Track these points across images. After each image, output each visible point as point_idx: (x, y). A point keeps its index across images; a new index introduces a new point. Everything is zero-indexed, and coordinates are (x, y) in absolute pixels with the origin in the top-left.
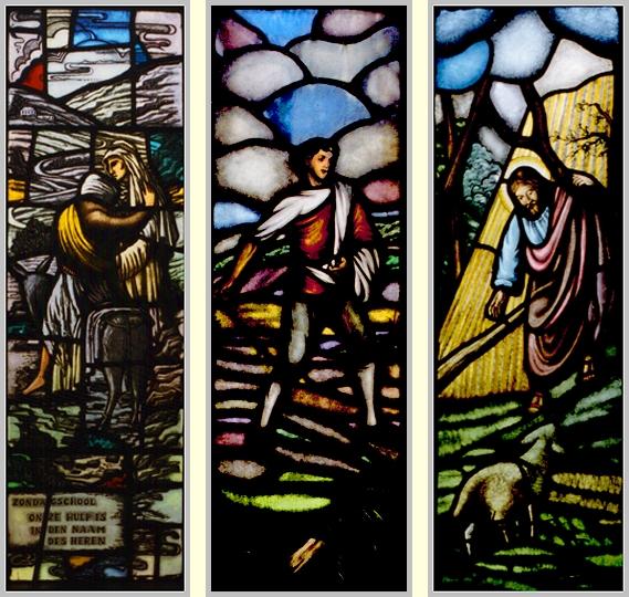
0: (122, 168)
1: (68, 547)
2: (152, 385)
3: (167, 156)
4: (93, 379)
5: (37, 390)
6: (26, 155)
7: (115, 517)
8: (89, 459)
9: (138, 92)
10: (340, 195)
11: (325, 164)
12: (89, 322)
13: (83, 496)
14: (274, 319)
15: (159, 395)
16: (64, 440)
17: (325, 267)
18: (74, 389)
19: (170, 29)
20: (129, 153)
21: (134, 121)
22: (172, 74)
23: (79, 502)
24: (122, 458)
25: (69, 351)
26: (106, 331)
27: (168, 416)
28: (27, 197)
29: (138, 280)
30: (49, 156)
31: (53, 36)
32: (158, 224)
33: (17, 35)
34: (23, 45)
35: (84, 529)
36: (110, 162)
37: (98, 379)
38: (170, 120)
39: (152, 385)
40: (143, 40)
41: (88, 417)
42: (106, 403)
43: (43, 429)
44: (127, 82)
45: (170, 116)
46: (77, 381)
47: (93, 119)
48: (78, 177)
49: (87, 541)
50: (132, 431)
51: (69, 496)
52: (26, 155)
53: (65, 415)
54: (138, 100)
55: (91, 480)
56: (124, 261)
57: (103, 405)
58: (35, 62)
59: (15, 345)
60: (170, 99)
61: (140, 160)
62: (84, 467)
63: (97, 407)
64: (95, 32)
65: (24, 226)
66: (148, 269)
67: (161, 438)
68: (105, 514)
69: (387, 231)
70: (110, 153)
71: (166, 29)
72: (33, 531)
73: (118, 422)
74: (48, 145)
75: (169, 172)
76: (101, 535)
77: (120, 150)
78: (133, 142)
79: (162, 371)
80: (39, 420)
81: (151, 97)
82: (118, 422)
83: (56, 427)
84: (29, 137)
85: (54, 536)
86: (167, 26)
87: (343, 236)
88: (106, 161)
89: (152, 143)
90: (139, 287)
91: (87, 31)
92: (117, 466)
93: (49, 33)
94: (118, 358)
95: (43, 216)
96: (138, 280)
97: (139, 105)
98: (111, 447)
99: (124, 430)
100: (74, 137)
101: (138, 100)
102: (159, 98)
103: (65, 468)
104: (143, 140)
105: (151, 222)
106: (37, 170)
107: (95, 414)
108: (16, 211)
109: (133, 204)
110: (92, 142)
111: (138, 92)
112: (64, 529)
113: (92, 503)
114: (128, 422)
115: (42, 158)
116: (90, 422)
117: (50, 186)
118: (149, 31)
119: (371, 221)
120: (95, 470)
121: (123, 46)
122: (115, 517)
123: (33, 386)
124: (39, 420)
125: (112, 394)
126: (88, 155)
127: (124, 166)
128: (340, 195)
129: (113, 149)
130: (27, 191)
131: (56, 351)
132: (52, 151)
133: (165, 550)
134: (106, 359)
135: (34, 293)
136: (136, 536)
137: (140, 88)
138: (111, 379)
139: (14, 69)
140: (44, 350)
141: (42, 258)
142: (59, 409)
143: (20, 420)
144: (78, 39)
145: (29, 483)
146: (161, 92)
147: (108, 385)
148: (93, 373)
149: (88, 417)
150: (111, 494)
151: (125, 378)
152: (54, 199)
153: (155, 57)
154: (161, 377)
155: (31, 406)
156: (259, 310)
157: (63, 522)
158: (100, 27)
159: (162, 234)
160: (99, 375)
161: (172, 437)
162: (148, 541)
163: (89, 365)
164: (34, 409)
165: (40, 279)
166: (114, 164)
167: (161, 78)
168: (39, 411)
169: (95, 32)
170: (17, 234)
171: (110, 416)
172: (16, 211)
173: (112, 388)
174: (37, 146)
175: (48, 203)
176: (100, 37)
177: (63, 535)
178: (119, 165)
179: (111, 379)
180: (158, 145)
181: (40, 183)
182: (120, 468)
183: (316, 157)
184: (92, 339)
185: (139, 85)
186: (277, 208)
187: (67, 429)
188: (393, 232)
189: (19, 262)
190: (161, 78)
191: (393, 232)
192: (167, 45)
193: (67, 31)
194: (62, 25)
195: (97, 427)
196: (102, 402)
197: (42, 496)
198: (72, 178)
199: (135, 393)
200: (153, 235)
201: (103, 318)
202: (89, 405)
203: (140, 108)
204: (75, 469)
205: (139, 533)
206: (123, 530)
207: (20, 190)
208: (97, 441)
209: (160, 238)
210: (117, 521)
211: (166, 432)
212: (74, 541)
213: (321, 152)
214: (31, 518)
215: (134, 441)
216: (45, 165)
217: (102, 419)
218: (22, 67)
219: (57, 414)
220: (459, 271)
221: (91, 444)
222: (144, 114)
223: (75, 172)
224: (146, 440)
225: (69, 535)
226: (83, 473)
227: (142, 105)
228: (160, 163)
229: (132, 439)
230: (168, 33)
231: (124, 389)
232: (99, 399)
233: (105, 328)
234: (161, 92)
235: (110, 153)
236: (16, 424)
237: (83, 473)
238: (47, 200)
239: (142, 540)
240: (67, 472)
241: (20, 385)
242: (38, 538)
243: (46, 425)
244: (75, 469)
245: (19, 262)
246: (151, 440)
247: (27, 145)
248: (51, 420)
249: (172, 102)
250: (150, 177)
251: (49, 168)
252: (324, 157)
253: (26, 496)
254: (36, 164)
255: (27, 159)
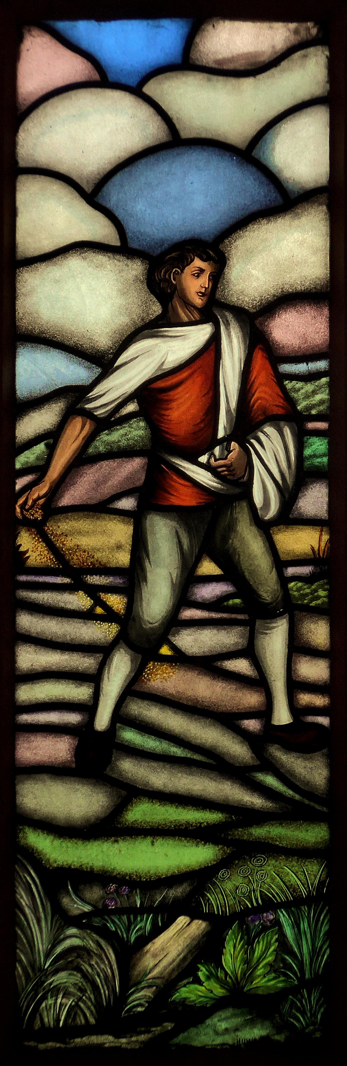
10: (229, 336)
11: (204, 281)
14: (119, 547)
17: (203, 459)
29: (220, 469)
69: (307, 396)
87: (233, 404)
96: (220, 469)
119: (284, 581)
128: (229, 336)
133: (319, 418)
156: (94, 533)
183: (188, 270)
186: (118, 363)
188: (318, 397)
191: (318, 397)
213: (198, 263)
252: (202, 271)
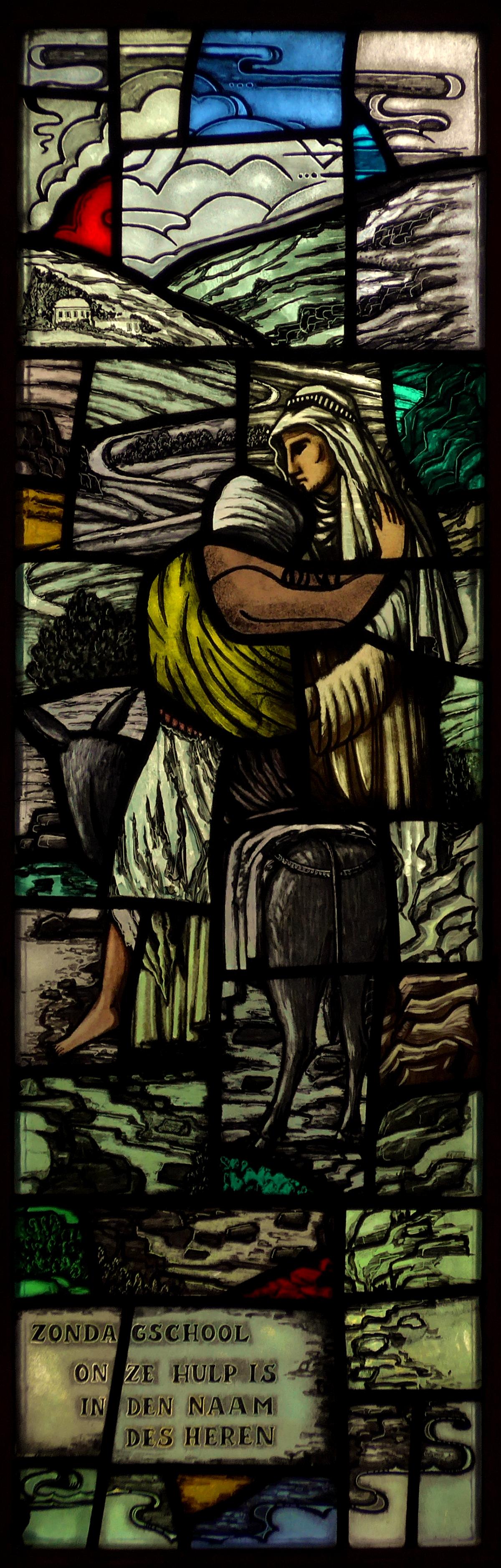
0: (320, 459)
1: (178, 1453)
2: (396, 1026)
3: (437, 426)
4: (240, 1012)
5: (97, 1041)
6: (66, 425)
7: (300, 1372)
8: (231, 1221)
9: (360, 255)
12: (232, 860)
13: (217, 1316)
15: (415, 1053)
16: (167, 1172)
18: (190, 1036)
19: (448, 86)
20: (337, 419)
21: (351, 332)
22: (453, 205)
23: (206, 1334)
24: (316, 1217)
25: (178, 936)
26: (278, 885)
27: (438, 1110)
28: (68, 533)
29: (362, 751)
30: (128, 426)
31: (138, 108)
32: (412, 603)
33: (42, 104)
34: (57, 131)
35: (219, 1406)
36: (288, 443)
37: (254, 1014)
38: (447, 330)
39: (396, 1026)
40: (376, 114)
41: (229, 1112)
42: (274, 1074)
43: (109, 1145)
44: (379, 379)
45: (447, 319)
46: (199, 1017)
47: (248, 329)
48: (203, 483)
49: (226, 1435)
50: (343, 1147)
51: (178, 1317)
52: (66, 425)
53: (168, 1107)
54: (362, 276)
55: (237, 1276)
56: (325, 701)
57: (268, 1081)
58: (91, 177)
59: (38, 923)
60: (446, 273)
61: (364, 436)
62: (217, 1240)
63: (254, 1085)
64: (250, 95)
65: (60, 611)
66: (387, 722)
67: (420, 1168)
68: (274, 1363)
70: (289, 420)
71: (439, 85)
72: (84, 1406)
73: (306, 1125)
74: (123, 398)
75: (443, 466)
76: (263, 1419)
77: (310, 411)
78: (346, 389)
79: (423, 992)
80: (100, 1121)
81: (396, 269)
82: (306, 1125)
83: (143, 1140)
84: (74, 377)
85: (142, 1423)
86: (441, 76)
88: (278, 440)
89: (399, 390)
90: (364, 769)
91: (229, 94)
92: (304, 1239)
93: (126, 98)
94: (309, 954)
95: (109, 584)
96: (362, 751)
97: (364, 291)
98: (287, 1190)
99: (323, 1146)
100: (194, 377)
101: (362, 276)
102: (417, 271)
103: (169, 1243)
104: (375, 383)
105: (395, 598)
106: (96, 460)
107: (247, 1103)
108: (37, 573)
109: (349, 554)
110: (241, 391)
111: (360, 255)
112: (166, 1403)
113: (240, 1336)
114: (335, 1124)
115: (109, 431)
116: (232, 1124)
117: (127, 505)
118: (393, 92)
120: (245, 1250)
121: (323, 135)
122: (300, 1372)
123: (86, 1030)
124: (100, 1121)
125: (291, 1054)
126: (229, 423)
127: (324, 453)
129: (296, 408)
130: (67, 521)
131: (145, 933)
132: (135, 413)
133: (433, 1462)
134: (277, 959)
135: (90, 787)
136: (358, 1425)
137: (369, 245)
138: (287, 1013)
139: (35, 196)
140: (113, 933)
141: (106, 695)
142: (152, 1090)
143: (49, 1121)
144: (201, 115)
145: (74, 1283)
146: (424, 257)
147: (280, 1027)
148: (240, 997)
149: (229, 1112)
150: (290, 1314)
151: (323, 1008)
152: (139, 541)
153: (414, 159)
154: (418, 1007)
155: (78, 1084)
157: (165, 1386)
158: (260, 84)
159: (424, 630)
160: (256, 1001)
161: (450, 1168)
162: (391, 1436)
163: (235, 976)
164: (85, 1093)
165: (102, 749)
166: (298, 448)
167: (423, 219)
168: (98, 1098)
169: (250, 95)
170: (43, 631)
171: (284, 1111)
172: (37, 573)
173: (292, 1034)
174: (95, 401)
175: (125, 550)
176: (260, 111)
177: (166, 1421)
178: (310, 453)
179: (287, 1013)
180: (416, 396)
181: (105, 498)
182: (312, 1244)
184: (239, 907)
185: (363, 236)
187: (173, 1143)
189: (46, 707)
190: (423, 219)
192: (441, 128)
193: (176, 93)
194: (161, 76)
195: (253, 1138)
196: (267, 1073)
197: (108, 1317)
198: (186, 484)
199: (351, 1048)
200: (401, 632)
201: (270, 850)
202: (233, 1079)
203: (366, 299)
204: (194, 1246)
205: (366, 1416)
206: (323, 1407)
207: (49, 518)
208: (250, 1175)
209: (420, 641)
210: (307, 1383)
211: (434, 1153)
212: (193, 1436)
214: (78, 1373)
215: (350, 1174)
216: (115, 450)
217: (263, 1118)
218: (57, 190)
219: (145, 1103)
220: (162, 550)
221: (236, 1184)
222: (377, 313)
223: (195, 470)
224: (380, 1174)
225: (180, 1420)
226: (216, 1256)
227: (374, 289)
228: (416, 442)
229: (345, 1169)
230: (442, 96)
231: (321, 1037)
232: (259, 1064)
233: (273, 876)
234: (424, 257)
235: (289, 420)
236: (39, 1133)
237: (216, 1256)
238: (119, 543)
239: (375, 1431)
240: (173, 1255)
241: (50, 1030)
242: (98, 1426)
243: (118, 1134)
244: (194, 1246)
245: (46, 707)
246: (394, 1172)
247: (68, 398)
248: (132, 1120)
249: (451, 282)
250: (394, 484)
251: (128, 458)
253: (66, 1317)
254: (92, 448)
255: (67, 435)
